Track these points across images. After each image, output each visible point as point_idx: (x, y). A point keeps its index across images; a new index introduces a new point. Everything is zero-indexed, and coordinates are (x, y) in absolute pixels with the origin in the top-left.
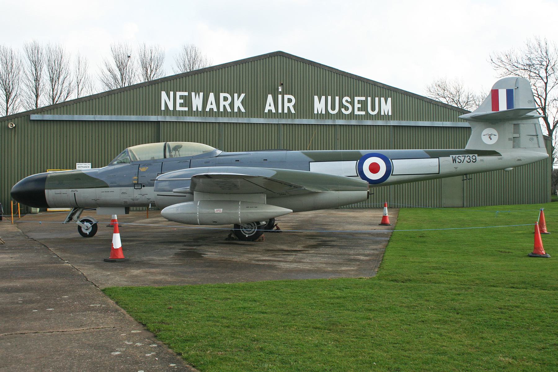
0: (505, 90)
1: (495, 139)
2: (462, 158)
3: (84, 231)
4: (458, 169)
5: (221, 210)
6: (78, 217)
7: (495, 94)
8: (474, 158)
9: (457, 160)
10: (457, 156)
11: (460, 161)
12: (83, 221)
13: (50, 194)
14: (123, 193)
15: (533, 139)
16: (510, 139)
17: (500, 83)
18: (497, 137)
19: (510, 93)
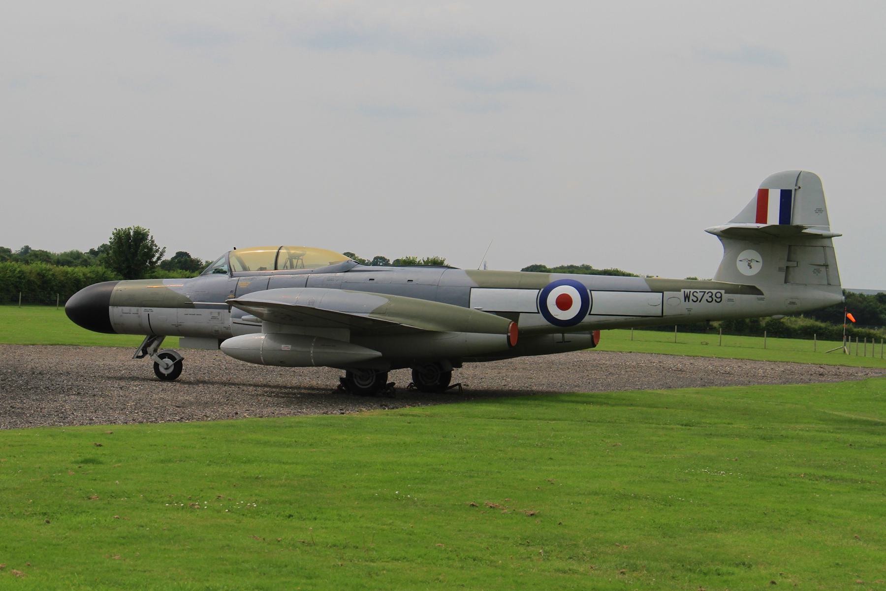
0: (779, 192)
1: (757, 268)
2: (699, 295)
3: (162, 370)
4: (692, 312)
5: (290, 346)
6: (155, 350)
7: (763, 196)
8: (718, 295)
9: (692, 297)
10: (692, 291)
11: (695, 299)
12: (162, 356)
13: (115, 312)
14: (214, 318)
15: (819, 271)
16: (780, 269)
17: (775, 180)
18: (760, 265)
19: (786, 197)
